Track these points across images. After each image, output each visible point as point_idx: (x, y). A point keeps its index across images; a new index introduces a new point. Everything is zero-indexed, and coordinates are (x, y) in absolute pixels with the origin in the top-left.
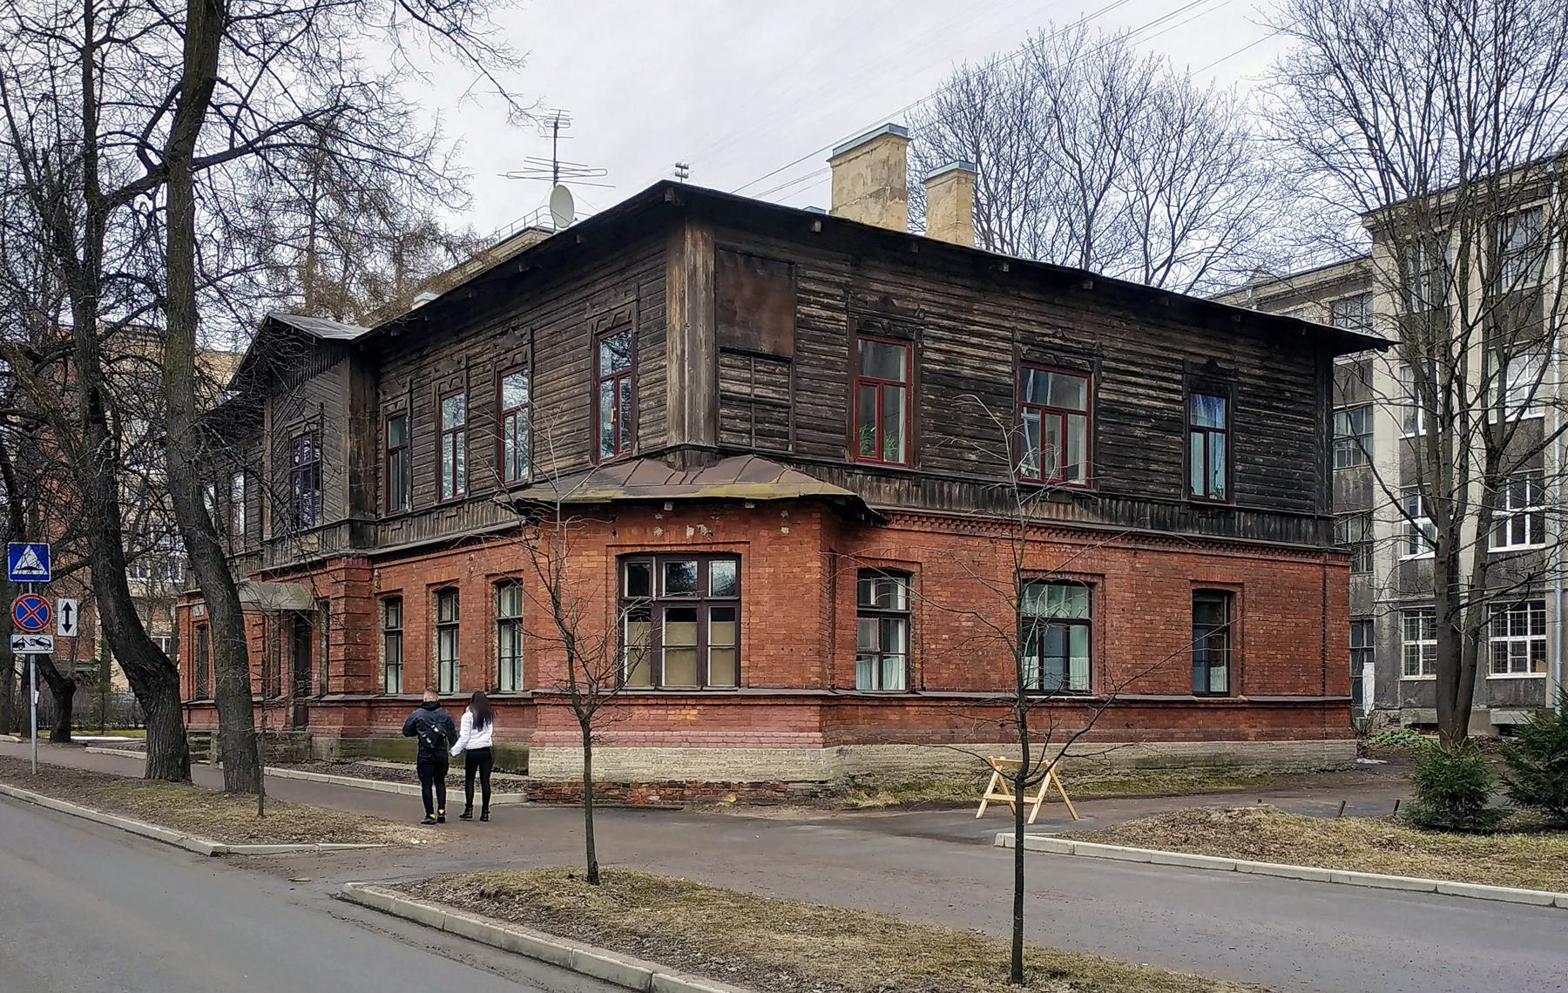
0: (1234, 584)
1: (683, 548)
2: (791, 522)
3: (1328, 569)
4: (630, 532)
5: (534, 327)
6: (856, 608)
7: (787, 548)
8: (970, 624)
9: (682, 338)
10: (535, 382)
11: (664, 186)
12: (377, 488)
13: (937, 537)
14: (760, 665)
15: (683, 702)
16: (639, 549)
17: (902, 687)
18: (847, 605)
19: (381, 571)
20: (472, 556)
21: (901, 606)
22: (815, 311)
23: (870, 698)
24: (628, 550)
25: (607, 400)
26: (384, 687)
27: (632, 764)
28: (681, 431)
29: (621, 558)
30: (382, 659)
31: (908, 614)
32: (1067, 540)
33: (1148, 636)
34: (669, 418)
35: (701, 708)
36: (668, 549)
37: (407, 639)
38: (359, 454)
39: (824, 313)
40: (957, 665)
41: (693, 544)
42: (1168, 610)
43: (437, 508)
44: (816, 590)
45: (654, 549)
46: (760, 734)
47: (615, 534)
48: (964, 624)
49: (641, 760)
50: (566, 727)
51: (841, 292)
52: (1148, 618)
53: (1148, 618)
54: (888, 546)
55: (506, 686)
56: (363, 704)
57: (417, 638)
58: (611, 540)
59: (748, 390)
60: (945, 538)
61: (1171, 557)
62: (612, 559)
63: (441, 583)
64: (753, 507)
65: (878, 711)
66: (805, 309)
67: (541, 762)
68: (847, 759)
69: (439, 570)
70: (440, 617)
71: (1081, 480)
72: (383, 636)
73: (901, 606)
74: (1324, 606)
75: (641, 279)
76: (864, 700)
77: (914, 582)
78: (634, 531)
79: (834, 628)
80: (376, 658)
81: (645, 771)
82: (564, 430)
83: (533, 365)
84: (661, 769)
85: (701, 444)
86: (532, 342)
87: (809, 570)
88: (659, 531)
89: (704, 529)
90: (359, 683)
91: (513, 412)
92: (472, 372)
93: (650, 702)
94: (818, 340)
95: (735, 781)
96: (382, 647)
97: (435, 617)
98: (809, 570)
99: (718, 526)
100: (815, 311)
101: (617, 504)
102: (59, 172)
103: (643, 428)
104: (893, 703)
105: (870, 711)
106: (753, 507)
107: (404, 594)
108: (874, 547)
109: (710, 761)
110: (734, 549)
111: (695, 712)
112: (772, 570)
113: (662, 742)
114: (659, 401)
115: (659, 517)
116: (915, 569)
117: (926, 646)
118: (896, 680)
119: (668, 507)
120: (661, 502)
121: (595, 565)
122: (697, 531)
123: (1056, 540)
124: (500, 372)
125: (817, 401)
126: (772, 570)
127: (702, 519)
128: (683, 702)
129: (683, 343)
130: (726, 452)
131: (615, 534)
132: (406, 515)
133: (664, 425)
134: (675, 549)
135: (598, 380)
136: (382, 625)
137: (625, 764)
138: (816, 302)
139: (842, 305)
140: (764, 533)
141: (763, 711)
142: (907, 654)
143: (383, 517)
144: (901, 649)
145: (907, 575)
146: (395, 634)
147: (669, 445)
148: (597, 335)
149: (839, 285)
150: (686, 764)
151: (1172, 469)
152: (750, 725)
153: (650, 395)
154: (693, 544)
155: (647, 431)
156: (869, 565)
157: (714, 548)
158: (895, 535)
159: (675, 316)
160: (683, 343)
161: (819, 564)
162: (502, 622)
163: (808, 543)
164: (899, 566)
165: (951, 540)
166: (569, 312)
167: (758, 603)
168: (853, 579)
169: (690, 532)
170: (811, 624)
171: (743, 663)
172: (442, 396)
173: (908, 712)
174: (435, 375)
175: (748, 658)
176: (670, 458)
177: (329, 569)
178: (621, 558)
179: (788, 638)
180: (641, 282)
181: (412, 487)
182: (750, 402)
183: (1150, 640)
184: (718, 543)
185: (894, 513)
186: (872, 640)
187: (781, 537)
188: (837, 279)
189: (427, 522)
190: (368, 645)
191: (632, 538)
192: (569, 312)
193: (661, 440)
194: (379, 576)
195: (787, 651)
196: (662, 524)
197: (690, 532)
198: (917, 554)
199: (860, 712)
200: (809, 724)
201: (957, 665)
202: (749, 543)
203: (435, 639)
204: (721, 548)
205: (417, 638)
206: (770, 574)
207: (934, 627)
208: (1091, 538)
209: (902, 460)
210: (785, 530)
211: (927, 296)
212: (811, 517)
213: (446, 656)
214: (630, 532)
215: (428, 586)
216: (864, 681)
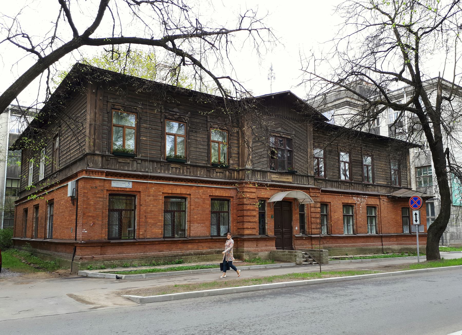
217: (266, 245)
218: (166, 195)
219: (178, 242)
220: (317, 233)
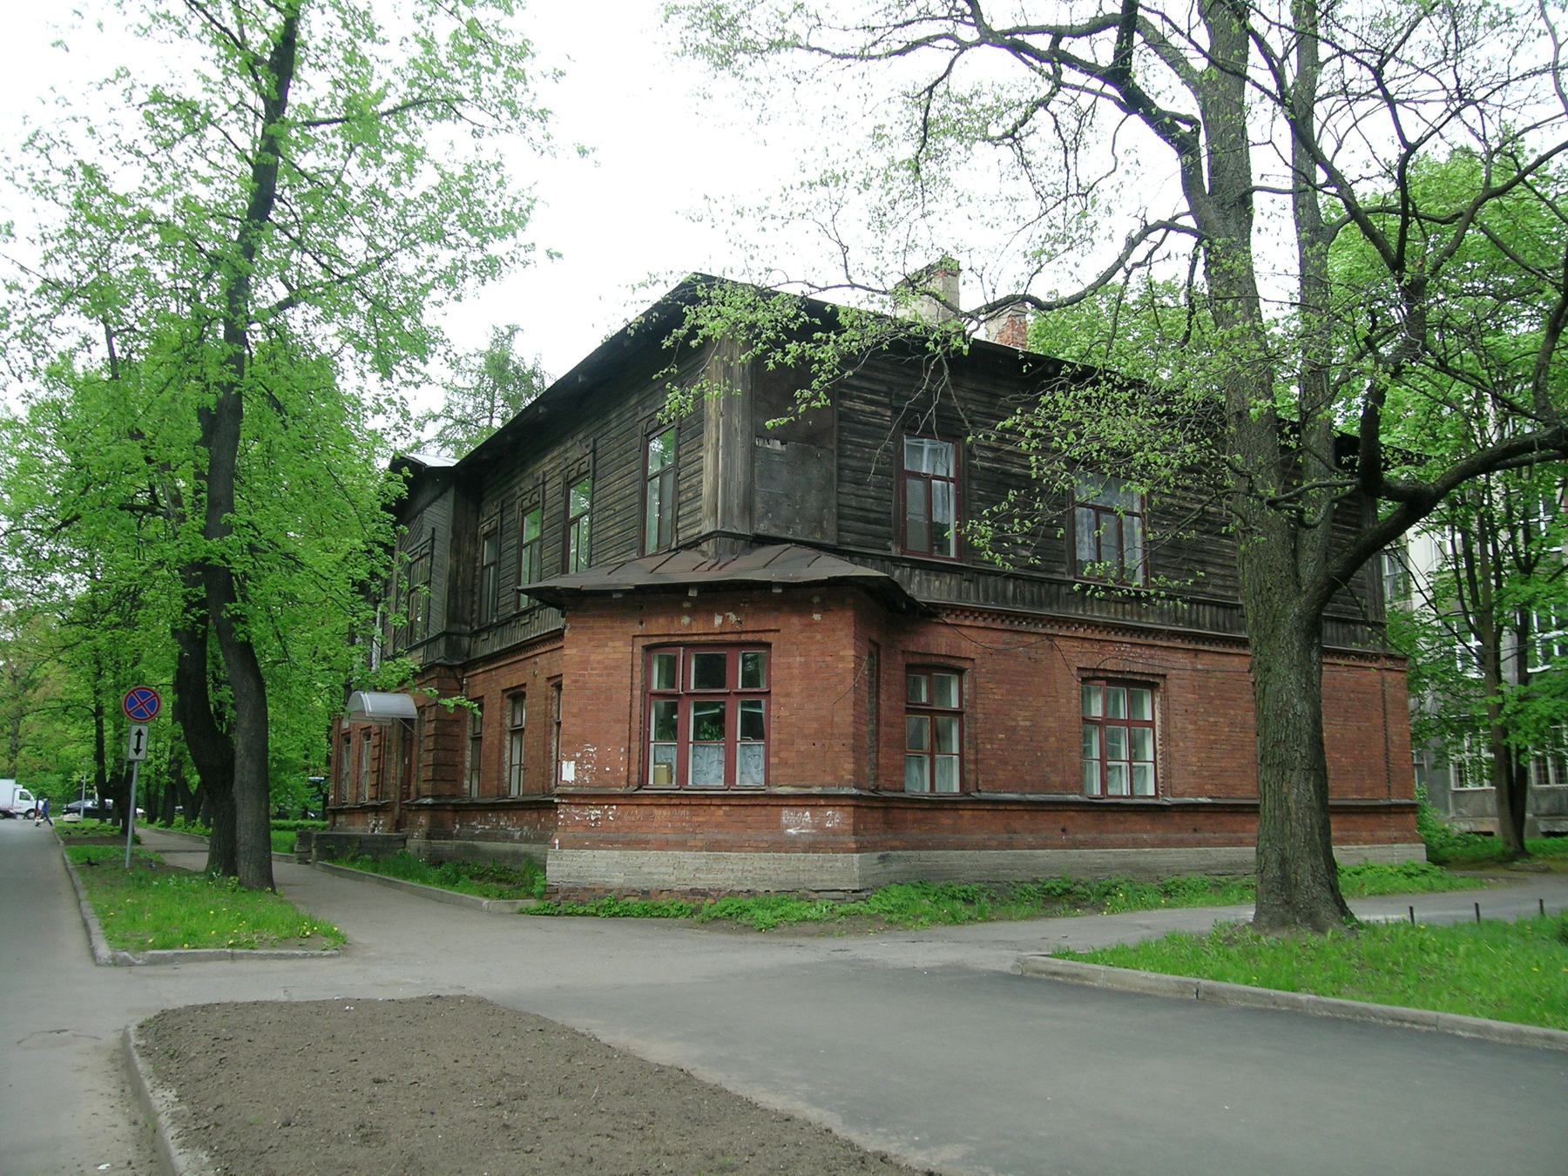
0: (1158, 675)
1: (711, 638)
2: (824, 608)
3: (1386, 673)
6: (904, 705)
7: (819, 637)
8: (1028, 723)
9: (717, 426)
10: (597, 488)
12: (473, 602)
13: (991, 634)
14: (790, 762)
15: (708, 802)
16: (665, 639)
17: (956, 789)
18: (889, 702)
21: (955, 704)
22: (858, 406)
23: (920, 801)
24: (655, 640)
25: (653, 499)
29: (648, 649)
30: (468, 764)
31: (962, 713)
32: (1127, 639)
33: (1212, 738)
34: (705, 508)
35: (727, 808)
36: (696, 638)
37: (486, 743)
38: (457, 572)
39: (868, 408)
40: (1015, 766)
41: (721, 633)
42: (1232, 712)
43: (515, 616)
44: (850, 681)
45: (681, 639)
47: (641, 623)
48: (1021, 723)
49: (662, 865)
51: (884, 389)
52: (1212, 719)
53: (1212, 719)
54: (940, 640)
55: (514, 792)
56: (449, 808)
57: (492, 743)
60: (999, 634)
61: (1232, 658)
62: (638, 650)
63: (513, 688)
64: (780, 591)
65: (929, 814)
66: (848, 404)
67: (559, 865)
68: (894, 867)
69: (510, 679)
70: (513, 720)
71: (1138, 581)
72: (469, 742)
73: (955, 704)
74: (1384, 709)
76: (915, 803)
77: (966, 679)
79: (878, 724)
80: (463, 763)
81: (666, 877)
82: (617, 530)
83: (595, 472)
84: (683, 876)
85: (735, 531)
86: (594, 451)
87: (842, 659)
89: (733, 617)
90: (446, 788)
91: (576, 520)
92: (547, 487)
93: (673, 802)
94: (863, 435)
96: (468, 753)
97: (508, 721)
98: (842, 659)
100: (858, 406)
101: (640, 589)
105: (920, 815)
106: (780, 591)
108: (923, 640)
110: (765, 638)
111: (721, 812)
112: (803, 659)
115: (686, 605)
116: (966, 665)
117: (981, 746)
118: (951, 784)
119: (692, 593)
120: (686, 586)
121: (620, 656)
122: (725, 619)
123: (1115, 638)
124: (569, 483)
125: (860, 493)
126: (803, 659)
128: (708, 802)
129: (718, 432)
130: (761, 541)
131: (641, 623)
132: (492, 625)
133: (699, 516)
134: (703, 638)
135: (646, 479)
136: (469, 733)
137: (646, 870)
138: (859, 398)
139: (886, 400)
140: (795, 620)
142: (961, 755)
144: (955, 749)
145: (960, 672)
146: (477, 739)
148: (647, 436)
149: (882, 382)
150: (709, 871)
151: (1228, 572)
153: (689, 487)
155: (686, 522)
156: (918, 660)
157: (744, 637)
158: (945, 630)
160: (718, 432)
161: (852, 653)
164: (952, 662)
165: (1006, 636)
167: (788, 695)
168: (900, 674)
169: (718, 620)
170: (844, 717)
171: (773, 760)
172: (525, 512)
173: (962, 816)
174: (519, 493)
175: (776, 754)
176: (704, 546)
178: (648, 649)
183: (1215, 742)
184: (747, 632)
185: (944, 607)
186: (1393, 917)
187: (812, 624)
188: (881, 376)
189: (507, 631)
190: (457, 751)
191: (659, 626)
193: (696, 530)
194: (468, 684)
196: (691, 613)
198: (967, 648)
199: (909, 815)
201: (1015, 766)
202: (778, 631)
203: (507, 744)
205: (492, 743)
207: (988, 726)
208: (1150, 638)
209: (953, 555)
210: (817, 617)
211: (973, 396)
213: (516, 760)
215: (504, 691)
216: (918, 783)
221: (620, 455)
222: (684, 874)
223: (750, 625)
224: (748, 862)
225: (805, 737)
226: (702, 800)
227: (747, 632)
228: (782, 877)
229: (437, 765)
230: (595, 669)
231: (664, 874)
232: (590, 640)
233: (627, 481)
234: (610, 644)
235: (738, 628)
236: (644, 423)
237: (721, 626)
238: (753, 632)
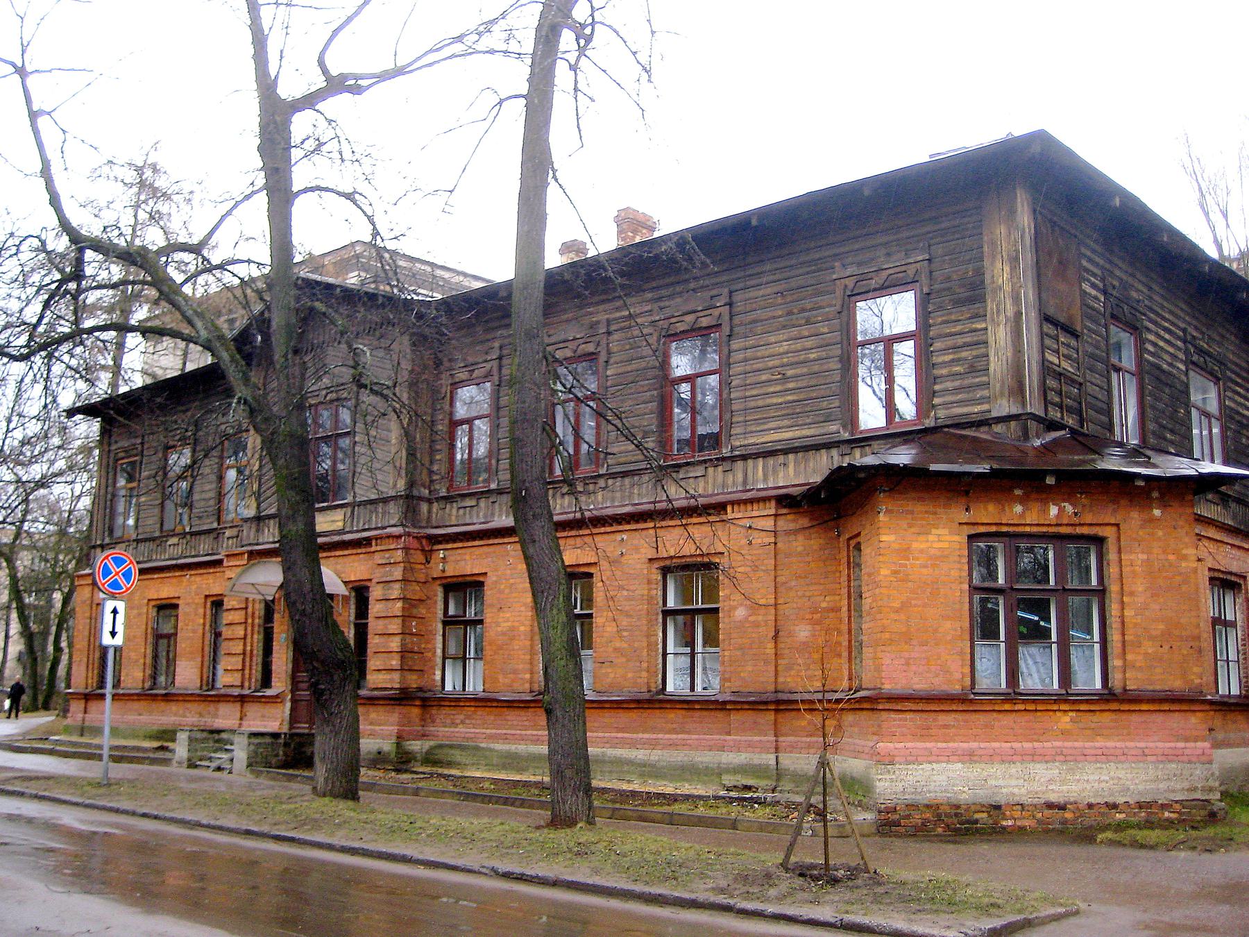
1: (1044, 529)
4: (986, 509)
5: (734, 287)
7: (1160, 533)
11: (1041, 137)
14: (1138, 664)
19: (447, 553)
20: (625, 537)
24: (982, 529)
26: (439, 683)
27: (1001, 782)
28: (1020, 398)
35: (1073, 714)
46: (1142, 745)
47: (967, 510)
50: (535, 726)
58: (964, 517)
59: (1056, 361)
72: (440, 626)
75: (932, 239)
78: (991, 507)
86: (730, 304)
88: (1018, 509)
89: (1069, 508)
95: (1120, 800)
99: (1084, 506)
102: (591, 24)
103: (940, 396)
104: (462, 704)
107: (489, 581)
109: (1091, 778)
110: (1101, 531)
112: (1145, 557)
113: (1034, 756)
114: (972, 366)
115: (1018, 492)
121: (946, 545)
122: (1061, 510)
126: (1145, 557)
127: (1066, 497)
128: (1055, 707)
137: (992, 782)
141: (1145, 717)
143: (443, 493)
147: (994, 414)
150: (1063, 782)
152: (1129, 734)
154: (1057, 525)
157: (1079, 530)
159: (1000, 274)
162: (667, 613)
163: (1182, 527)
166: (801, 271)
169: (1054, 510)
177: (373, 549)
179: (1167, 634)
180: (932, 242)
181: (498, 461)
182: (1060, 374)
187: (1152, 520)
191: (987, 514)
192: (801, 271)
193: (985, 407)
195: (1166, 647)
197: (1054, 510)
200: (1195, 733)
204: (1085, 530)
206: (1143, 561)
210: (1157, 512)
212: (1184, 498)
214: (986, 509)
217: (263, 716)
218: (153, 603)
219: (443, 703)
220: (384, 685)
221: (790, 313)
222: (1035, 787)
223: (1088, 518)
224: (1105, 772)
225: (1151, 638)
226: (1041, 701)
227: (1082, 525)
228: (1141, 787)
229: (404, 653)
230: (918, 559)
231: (1013, 787)
232: (910, 526)
233: (809, 343)
234: (934, 531)
235: (1076, 520)
236: (850, 283)
237: (1058, 516)
238: (1091, 525)
